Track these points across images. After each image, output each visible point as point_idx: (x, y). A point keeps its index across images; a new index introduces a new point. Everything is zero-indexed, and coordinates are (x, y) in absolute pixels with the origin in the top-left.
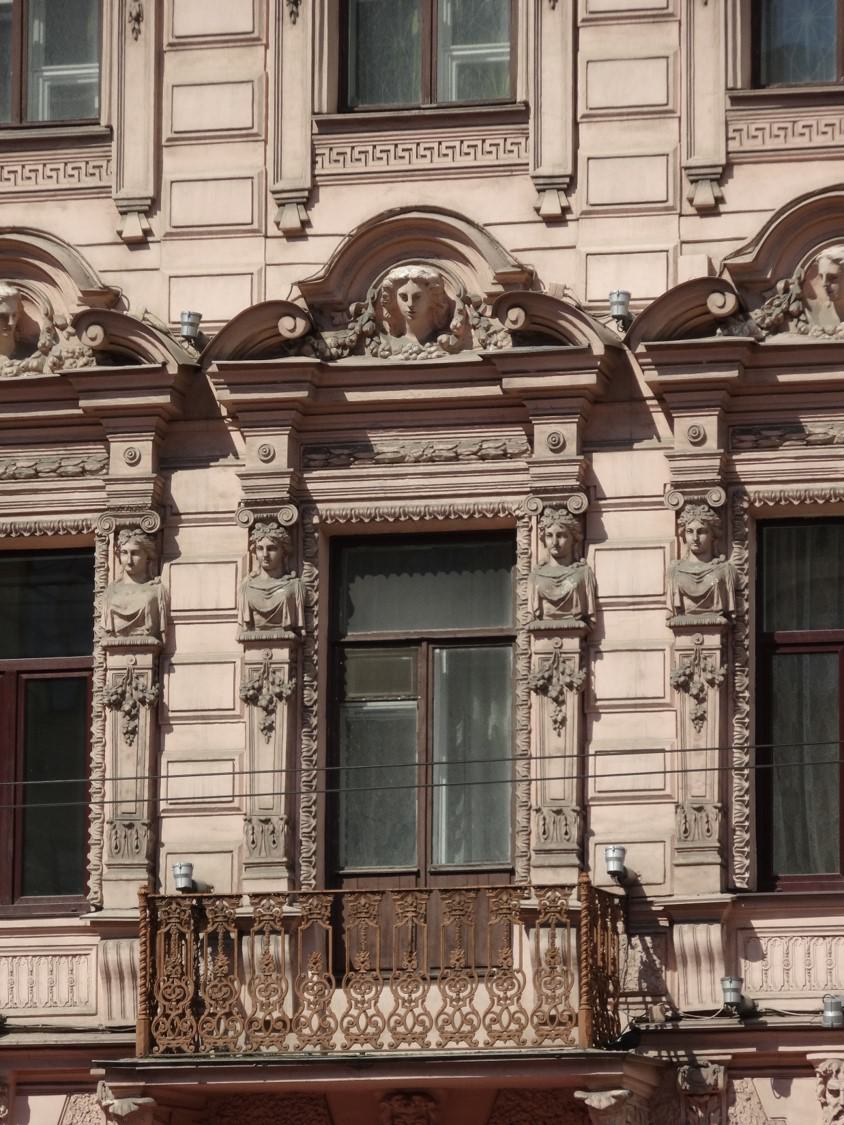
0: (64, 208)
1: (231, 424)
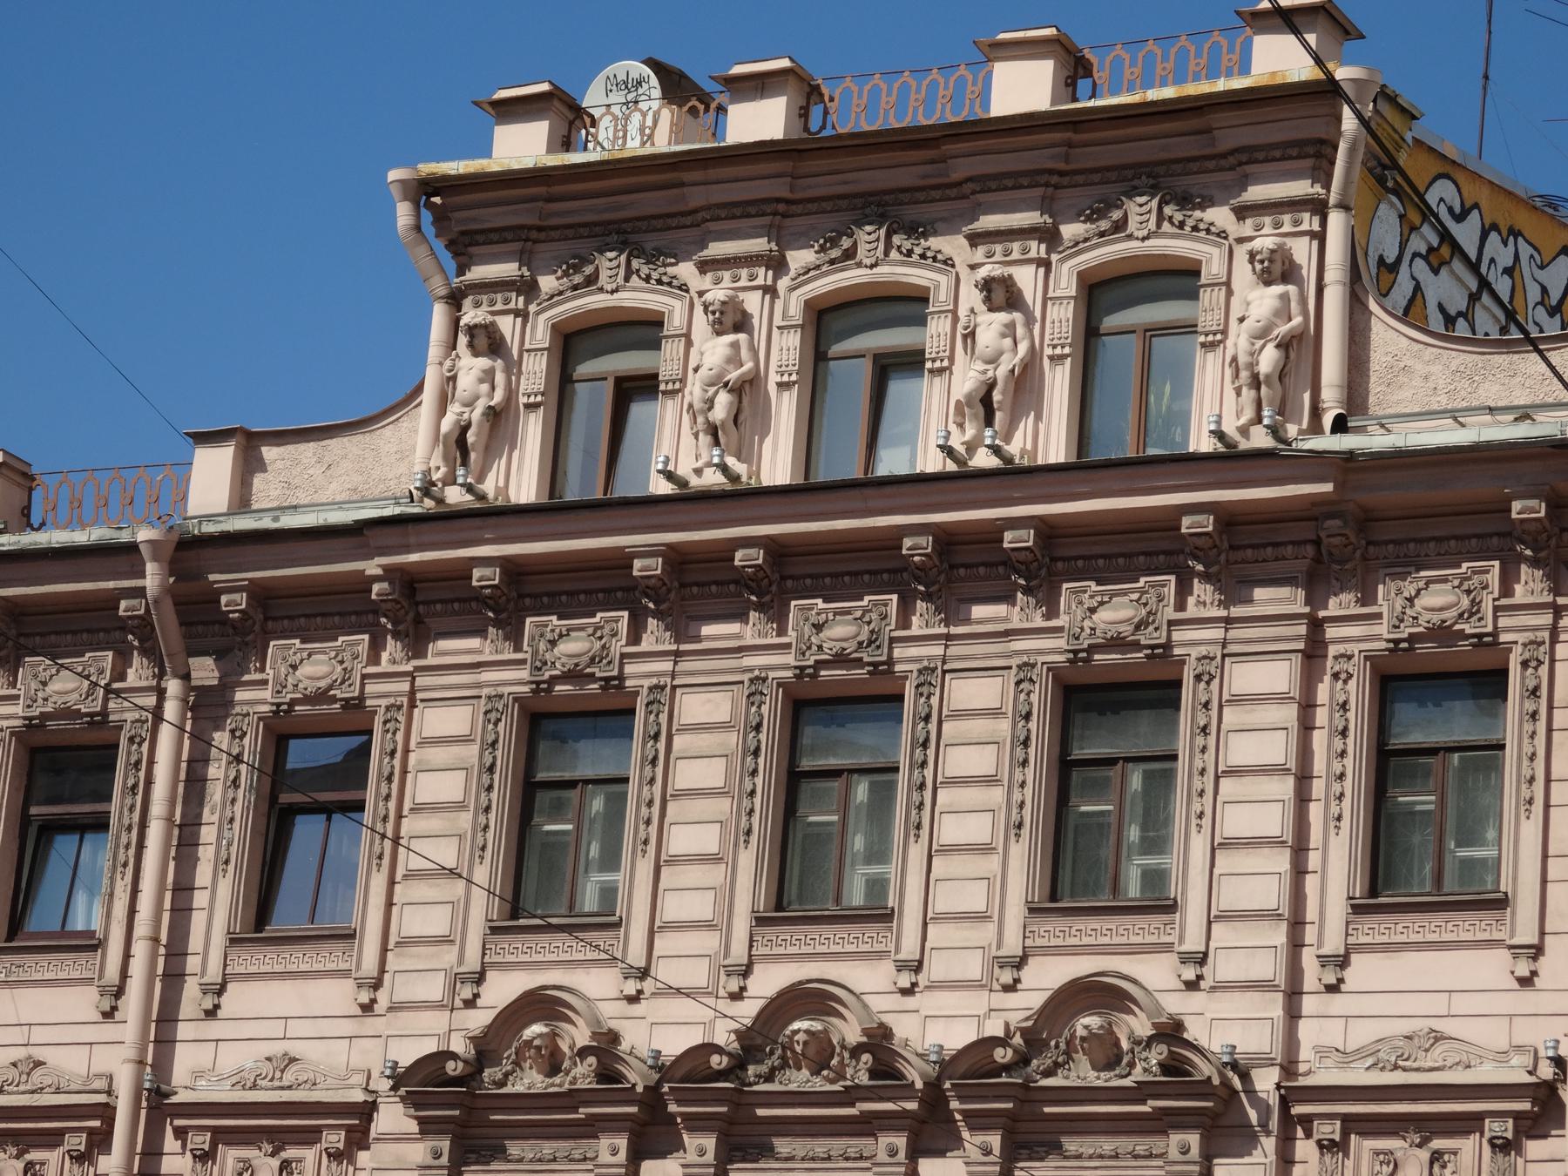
0: (588, 973)
1: (683, 1128)
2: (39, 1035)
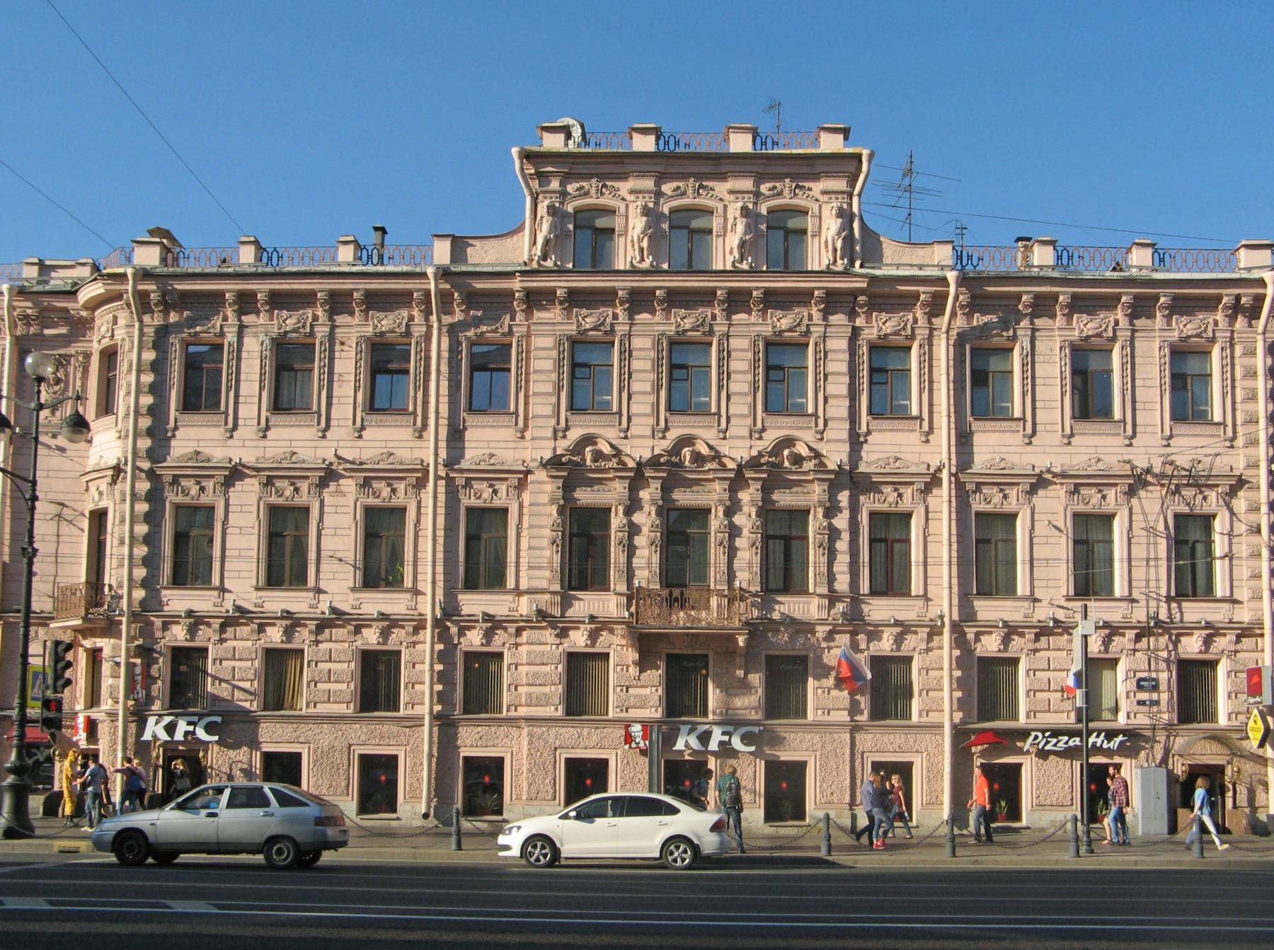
2: (389, 444)
